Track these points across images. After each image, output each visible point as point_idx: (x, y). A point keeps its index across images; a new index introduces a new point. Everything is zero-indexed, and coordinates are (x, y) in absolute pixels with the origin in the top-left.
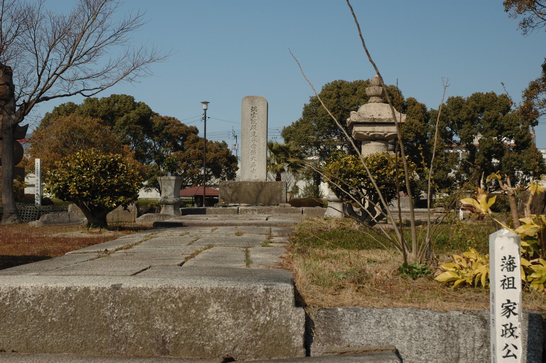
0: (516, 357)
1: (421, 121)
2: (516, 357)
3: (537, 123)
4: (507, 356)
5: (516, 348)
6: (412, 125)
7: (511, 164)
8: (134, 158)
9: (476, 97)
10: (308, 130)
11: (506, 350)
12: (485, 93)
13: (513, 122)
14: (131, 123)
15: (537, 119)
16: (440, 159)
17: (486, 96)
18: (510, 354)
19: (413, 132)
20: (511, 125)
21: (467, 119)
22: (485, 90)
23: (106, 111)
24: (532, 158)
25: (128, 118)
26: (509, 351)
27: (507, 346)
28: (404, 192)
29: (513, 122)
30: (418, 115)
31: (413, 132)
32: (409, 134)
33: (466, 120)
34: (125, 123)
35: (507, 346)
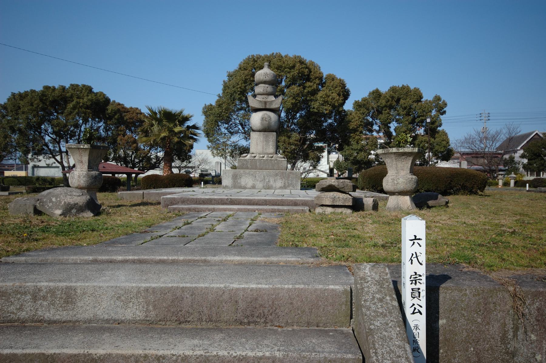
0: (421, 314)
1: (339, 95)
2: (421, 314)
3: (444, 112)
4: (413, 313)
5: (421, 307)
6: (329, 96)
7: (424, 146)
8: (205, 158)
9: (393, 89)
10: (222, 104)
11: (413, 308)
12: (401, 86)
13: (426, 109)
14: (81, 107)
15: (445, 109)
16: (358, 135)
17: (401, 88)
18: (416, 311)
19: (330, 105)
20: (424, 111)
21: (385, 106)
22: (399, 84)
23: (58, 96)
24: (443, 141)
25: (78, 103)
26: (415, 309)
27: (414, 305)
28: (292, 166)
29: (426, 109)
30: (337, 89)
31: (330, 105)
32: (325, 107)
33: (384, 107)
34: (74, 108)
35: (414, 305)
